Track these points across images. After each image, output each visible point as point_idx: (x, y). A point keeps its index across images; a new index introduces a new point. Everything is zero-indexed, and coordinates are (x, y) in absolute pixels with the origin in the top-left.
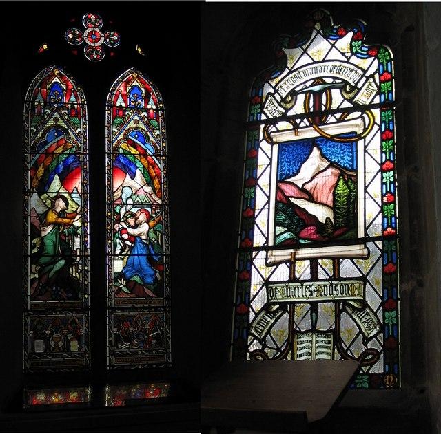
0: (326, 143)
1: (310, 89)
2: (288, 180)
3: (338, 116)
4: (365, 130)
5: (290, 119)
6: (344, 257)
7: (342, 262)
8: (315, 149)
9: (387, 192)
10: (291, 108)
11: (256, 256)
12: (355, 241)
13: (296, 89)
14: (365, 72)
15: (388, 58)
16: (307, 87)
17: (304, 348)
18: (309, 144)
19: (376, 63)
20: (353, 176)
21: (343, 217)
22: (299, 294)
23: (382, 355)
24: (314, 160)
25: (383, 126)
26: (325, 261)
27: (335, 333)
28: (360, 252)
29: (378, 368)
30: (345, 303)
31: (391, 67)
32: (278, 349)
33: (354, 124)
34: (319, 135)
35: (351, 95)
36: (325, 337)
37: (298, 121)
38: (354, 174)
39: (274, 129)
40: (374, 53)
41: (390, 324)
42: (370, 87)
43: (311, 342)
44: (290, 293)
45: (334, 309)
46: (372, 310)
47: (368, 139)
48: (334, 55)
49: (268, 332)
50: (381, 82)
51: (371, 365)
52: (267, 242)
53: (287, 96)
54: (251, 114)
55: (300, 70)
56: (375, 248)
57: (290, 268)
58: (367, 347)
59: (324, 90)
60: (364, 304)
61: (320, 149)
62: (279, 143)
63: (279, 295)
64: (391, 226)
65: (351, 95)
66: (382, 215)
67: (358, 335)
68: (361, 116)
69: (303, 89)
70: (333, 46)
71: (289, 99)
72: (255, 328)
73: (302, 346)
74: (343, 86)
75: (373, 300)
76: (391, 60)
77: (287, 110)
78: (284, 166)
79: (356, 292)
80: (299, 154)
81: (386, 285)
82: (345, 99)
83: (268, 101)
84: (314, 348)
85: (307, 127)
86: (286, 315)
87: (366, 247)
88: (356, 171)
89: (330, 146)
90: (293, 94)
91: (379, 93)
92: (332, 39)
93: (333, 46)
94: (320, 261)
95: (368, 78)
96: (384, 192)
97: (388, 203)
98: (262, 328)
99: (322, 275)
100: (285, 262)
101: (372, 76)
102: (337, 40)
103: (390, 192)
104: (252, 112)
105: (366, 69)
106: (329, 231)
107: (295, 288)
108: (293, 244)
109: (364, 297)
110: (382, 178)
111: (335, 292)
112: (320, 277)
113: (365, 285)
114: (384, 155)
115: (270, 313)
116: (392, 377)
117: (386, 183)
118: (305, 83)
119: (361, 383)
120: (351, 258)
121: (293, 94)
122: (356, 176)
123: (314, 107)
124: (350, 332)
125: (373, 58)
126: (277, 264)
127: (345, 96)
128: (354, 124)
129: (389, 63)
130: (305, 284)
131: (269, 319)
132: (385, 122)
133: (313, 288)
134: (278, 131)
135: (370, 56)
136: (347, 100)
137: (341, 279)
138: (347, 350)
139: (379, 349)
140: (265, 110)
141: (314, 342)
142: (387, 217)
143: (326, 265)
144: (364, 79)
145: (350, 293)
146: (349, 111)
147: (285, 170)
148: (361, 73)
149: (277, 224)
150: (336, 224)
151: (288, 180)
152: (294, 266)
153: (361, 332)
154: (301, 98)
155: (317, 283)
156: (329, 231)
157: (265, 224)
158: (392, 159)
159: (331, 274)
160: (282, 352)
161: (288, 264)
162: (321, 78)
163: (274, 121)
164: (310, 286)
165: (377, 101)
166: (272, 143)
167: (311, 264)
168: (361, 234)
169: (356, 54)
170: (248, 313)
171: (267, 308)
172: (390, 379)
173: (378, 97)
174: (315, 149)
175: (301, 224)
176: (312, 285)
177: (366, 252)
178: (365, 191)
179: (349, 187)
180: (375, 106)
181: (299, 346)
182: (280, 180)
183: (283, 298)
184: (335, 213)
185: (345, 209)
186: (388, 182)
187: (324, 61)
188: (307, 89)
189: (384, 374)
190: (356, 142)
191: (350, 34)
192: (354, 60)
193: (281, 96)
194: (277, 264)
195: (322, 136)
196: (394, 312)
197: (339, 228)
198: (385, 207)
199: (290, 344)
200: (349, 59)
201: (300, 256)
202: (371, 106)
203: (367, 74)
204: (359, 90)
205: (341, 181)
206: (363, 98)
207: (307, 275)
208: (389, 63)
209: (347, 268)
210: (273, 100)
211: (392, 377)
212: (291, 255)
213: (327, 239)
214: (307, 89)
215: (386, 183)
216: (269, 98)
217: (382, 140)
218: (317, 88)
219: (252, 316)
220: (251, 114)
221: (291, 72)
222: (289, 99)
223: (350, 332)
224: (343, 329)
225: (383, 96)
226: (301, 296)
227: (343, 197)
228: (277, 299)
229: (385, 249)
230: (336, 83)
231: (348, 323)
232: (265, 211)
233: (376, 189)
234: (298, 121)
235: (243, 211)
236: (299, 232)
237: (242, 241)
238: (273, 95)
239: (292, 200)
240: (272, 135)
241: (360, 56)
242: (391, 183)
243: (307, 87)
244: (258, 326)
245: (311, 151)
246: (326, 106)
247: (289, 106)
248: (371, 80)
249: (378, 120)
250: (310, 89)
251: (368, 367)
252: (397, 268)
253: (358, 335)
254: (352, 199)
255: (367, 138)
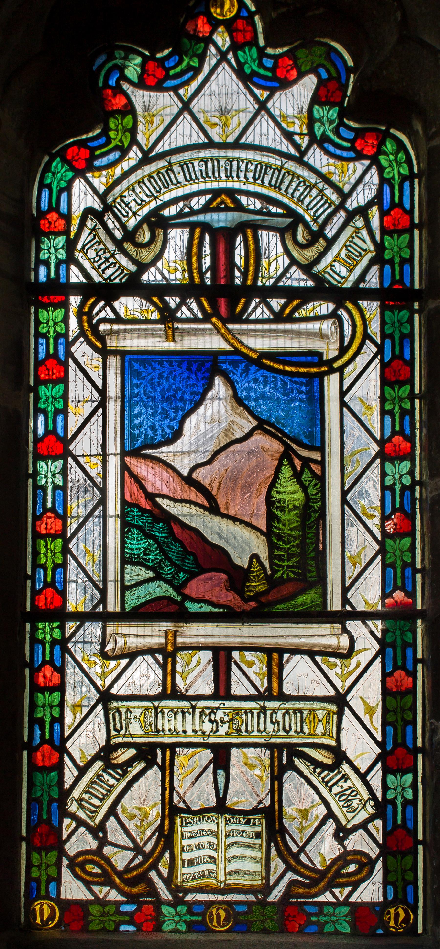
0: (246, 371)
1: (201, 218)
2: (150, 452)
3: (276, 304)
4: (343, 350)
5: (149, 292)
6: (294, 651)
7: (288, 661)
8: (218, 381)
9: (394, 510)
10: (153, 263)
11: (73, 634)
12: (320, 615)
13: (166, 212)
14: (345, 197)
15: (405, 171)
16: (193, 213)
17: (199, 847)
18: (206, 366)
19: (373, 177)
20: (315, 461)
21: (290, 556)
22: (189, 725)
23: (379, 865)
24: (214, 416)
25: (388, 343)
26: (249, 656)
27: (271, 817)
28: (333, 641)
29: (371, 891)
30: (294, 751)
31: (414, 196)
32: (137, 849)
33: (316, 331)
34: (229, 348)
35: (310, 253)
36: (248, 823)
37: (173, 302)
38: (316, 456)
39: (108, 313)
40: (369, 151)
41: (399, 801)
42: (356, 240)
43: (214, 834)
44: (164, 723)
45: (267, 762)
46: (356, 769)
47: (351, 373)
48: (264, 132)
49: (112, 811)
50: (384, 231)
51: (356, 885)
52: (103, 600)
53: (139, 226)
54: (39, 262)
55: (174, 159)
56: (365, 637)
57: (164, 667)
58: (344, 847)
59: (241, 228)
60: (339, 756)
61: (230, 383)
62: (123, 354)
63: (135, 728)
64: (403, 589)
65: (310, 253)
66: (383, 561)
67: (323, 823)
68: (333, 315)
69: (181, 215)
70: (262, 106)
71: (145, 236)
72: (80, 801)
73: (193, 842)
74: (290, 224)
75: (360, 746)
76: (411, 177)
77: (143, 267)
78: (139, 414)
79: (320, 729)
80: (179, 389)
81: (390, 718)
82: (293, 262)
83: (86, 232)
84: (222, 848)
85: (195, 320)
86: (154, 774)
87: (345, 631)
88: (321, 449)
89: (256, 381)
90: (158, 222)
91: (378, 259)
92: (259, 87)
93: (262, 106)
94: (236, 655)
95: (351, 216)
96: (388, 511)
97: (398, 535)
98: (96, 802)
99: (239, 686)
100: (152, 651)
101: (362, 211)
102: (272, 92)
103: (402, 509)
104: (44, 256)
105: (347, 189)
106: (258, 586)
107: (176, 714)
108: (171, 611)
109: (338, 740)
110: (384, 474)
111: (270, 727)
112: (237, 689)
113: (340, 714)
114: (388, 419)
115: (115, 767)
116: (400, 910)
117: (391, 488)
118: (187, 197)
119: (334, 923)
120: (312, 654)
121: (158, 222)
122: (322, 463)
123: (214, 268)
124: (304, 814)
125: (367, 162)
126: (132, 655)
127: (295, 254)
128: (316, 331)
129: (407, 185)
130: (201, 704)
131: (112, 782)
132: (391, 336)
133: (220, 714)
134: (119, 320)
135: (360, 156)
136: (300, 266)
137: (283, 698)
138: (299, 853)
139: (373, 851)
140: (79, 256)
141: (222, 848)
142: (393, 566)
143: (250, 664)
144: (341, 217)
145: (306, 730)
146: (304, 295)
147: (140, 426)
148: (334, 197)
149: (126, 560)
150: (274, 572)
151: (150, 452)
152: (174, 663)
153: (330, 814)
154: (178, 238)
155: (228, 704)
156: (258, 586)
157: (92, 556)
158: (408, 431)
159: (263, 685)
160: (147, 856)
161: (160, 657)
162: (231, 193)
163: (108, 292)
164: (213, 710)
165: (373, 281)
166: (105, 353)
167: (216, 660)
168: (335, 603)
169: (322, 142)
170: (60, 767)
171: (106, 754)
172: (397, 915)
173: (375, 269)
174: (218, 381)
175: (189, 565)
176: (218, 708)
177: (345, 641)
178: (344, 501)
179: (304, 489)
180: (370, 294)
181: (185, 842)
182: (132, 451)
183: (146, 735)
184: (272, 546)
185: (295, 538)
186: (398, 486)
187: (236, 145)
188: (194, 219)
189: (385, 904)
190: (321, 376)
191: (310, 82)
192: (317, 157)
193: (123, 226)
194: (132, 655)
195: (237, 352)
196: (409, 778)
197: (282, 581)
198: (389, 542)
199: (166, 837)
200: (303, 153)
201: (187, 640)
202: (357, 293)
203: (352, 204)
204: (330, 243)
205: (286, 471)
206: (337, 268)
207: (205, 687)
208: (407, 185)
209: (300, 676)
210: (102, 232)
211: (400, 910)
212: (166, 637)
213: (253, 604)
214: (194, 219)
215: (391, 488)
216: (90, 224)
217: (384, 382)
218: (220, 220)
219: (70, 774)
220: (39, 262)
221: (146, 159)
222: (145, 236)
223: (304, 814)
224: (289, 810)
225: (387, 268)
226: (190, 732)
227: (290, 510)
228: (132, 736)
229: (389, 640)
230: (269, 214)
231: (299, 795)
232: (95, 524)
233: (369, 494)
234: (173, 302)
235: (36, 518)
236: (185, 584)
237: (35, 593)
238: (99, 216)
239: (163, 502)
240: (103, 327)
241: (331, 148)
242: (404, 488)
243: (193, 213)
244: (86, 796)
245: (210, 386)
246: (245, 274)
247: (146, 255)
248: (359, 222)
249: (374, 328)
250: (201, 218)
251: (347, 890)
252: (413, 446)
253: (323, 823)
254: (313, 514)
255: (347, 370)
